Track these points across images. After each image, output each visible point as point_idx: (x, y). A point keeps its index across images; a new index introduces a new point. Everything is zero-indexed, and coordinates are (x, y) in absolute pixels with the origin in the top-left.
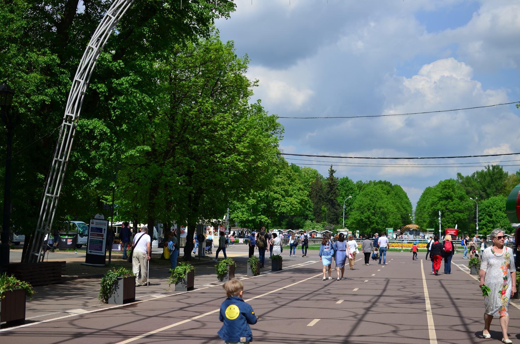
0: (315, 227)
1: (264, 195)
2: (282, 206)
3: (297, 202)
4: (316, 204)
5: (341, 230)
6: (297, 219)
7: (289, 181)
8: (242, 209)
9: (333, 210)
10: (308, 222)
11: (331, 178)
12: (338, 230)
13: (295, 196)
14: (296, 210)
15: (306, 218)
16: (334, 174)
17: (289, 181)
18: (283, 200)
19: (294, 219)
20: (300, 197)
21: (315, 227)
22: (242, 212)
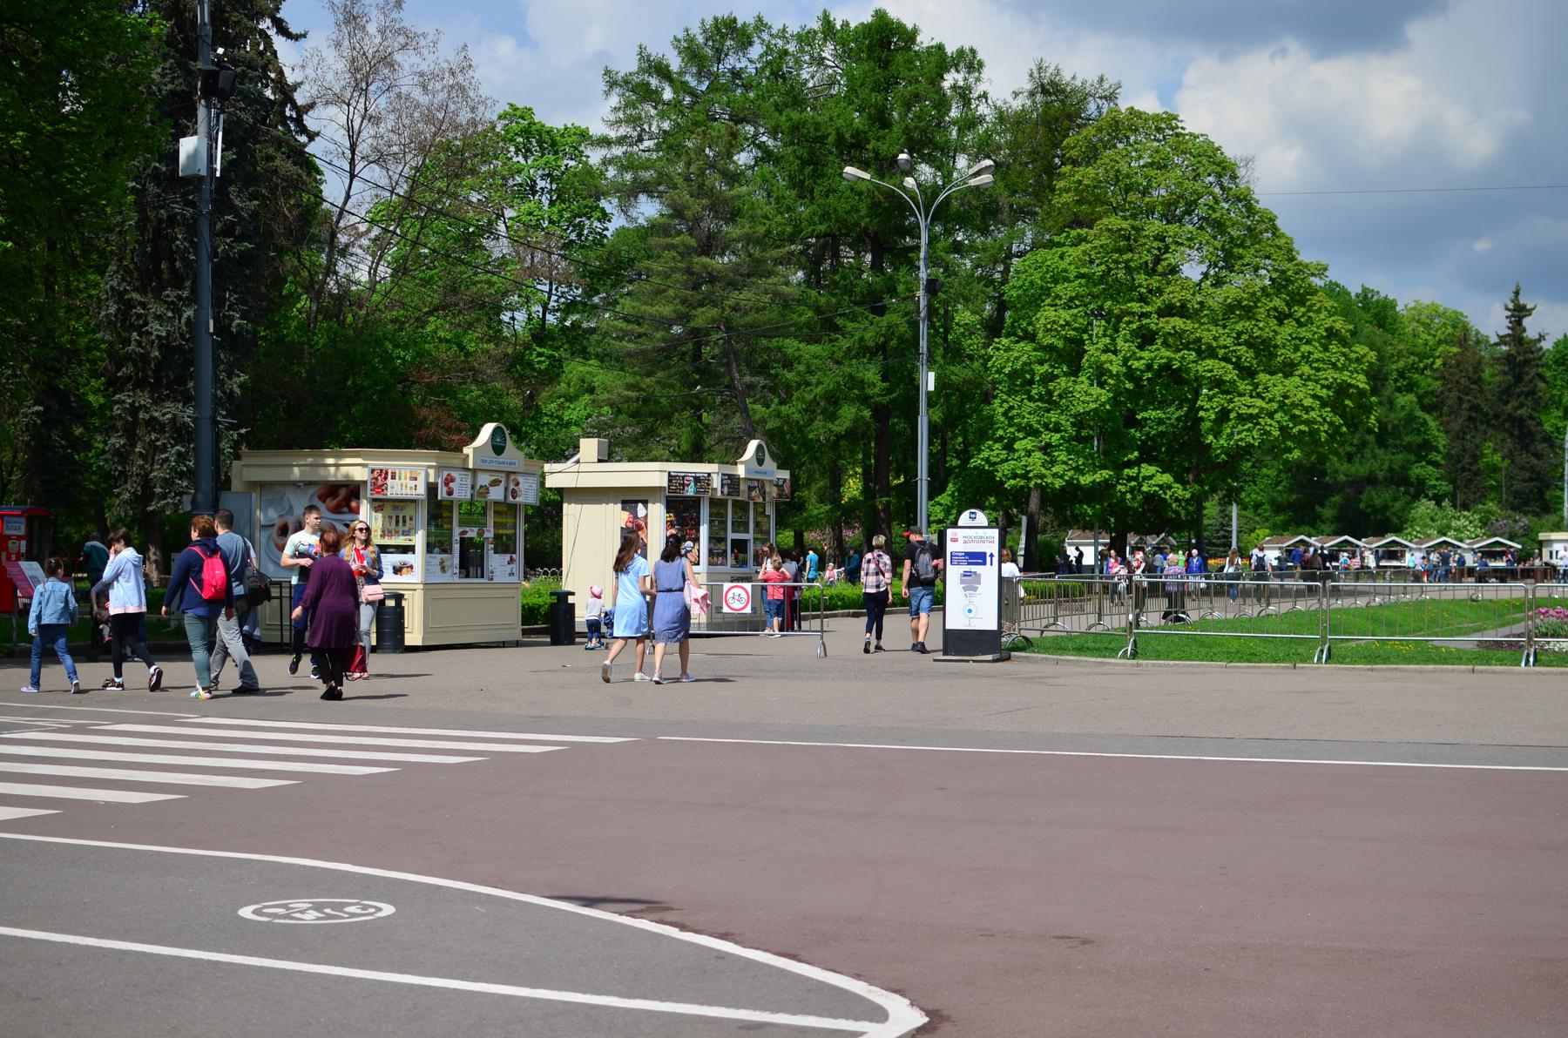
0: (1449, 527)
1: (1149, 367)
2: (1242, 419)
3: (1315, 397)
4: (1459, 436)
5: (1554, 536)
6: (1376, 497)
7: (1277, 302)
8: (1046, 437)
9: (1524, 458)
10: (1425, 507)
11: (1516, 335)
12: (1542, 536)
13: (1306, 369)
14: (1313, 434)
15: (1419, 490)
16: (1526, 322)
17: (1277, 302)
18: (1243, 386)
19: (1364, 497)
20: (1330, 375)
21: (1449, 527)
22: (1046, 449)
